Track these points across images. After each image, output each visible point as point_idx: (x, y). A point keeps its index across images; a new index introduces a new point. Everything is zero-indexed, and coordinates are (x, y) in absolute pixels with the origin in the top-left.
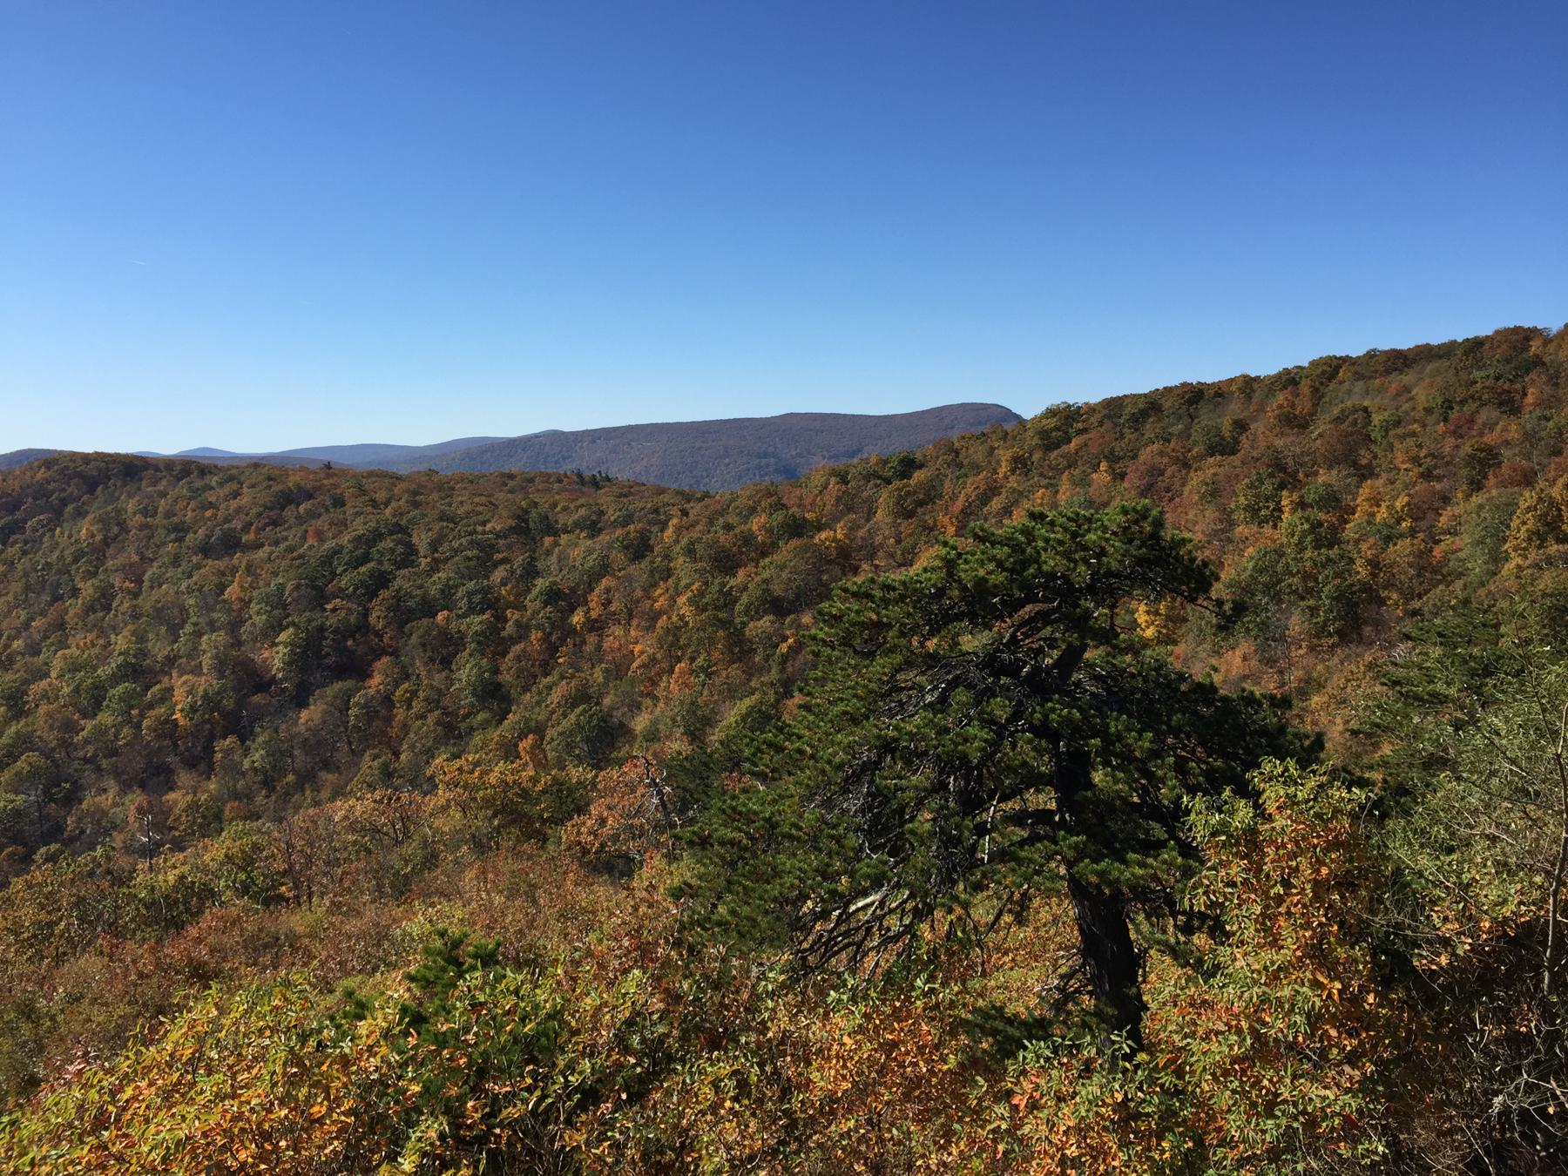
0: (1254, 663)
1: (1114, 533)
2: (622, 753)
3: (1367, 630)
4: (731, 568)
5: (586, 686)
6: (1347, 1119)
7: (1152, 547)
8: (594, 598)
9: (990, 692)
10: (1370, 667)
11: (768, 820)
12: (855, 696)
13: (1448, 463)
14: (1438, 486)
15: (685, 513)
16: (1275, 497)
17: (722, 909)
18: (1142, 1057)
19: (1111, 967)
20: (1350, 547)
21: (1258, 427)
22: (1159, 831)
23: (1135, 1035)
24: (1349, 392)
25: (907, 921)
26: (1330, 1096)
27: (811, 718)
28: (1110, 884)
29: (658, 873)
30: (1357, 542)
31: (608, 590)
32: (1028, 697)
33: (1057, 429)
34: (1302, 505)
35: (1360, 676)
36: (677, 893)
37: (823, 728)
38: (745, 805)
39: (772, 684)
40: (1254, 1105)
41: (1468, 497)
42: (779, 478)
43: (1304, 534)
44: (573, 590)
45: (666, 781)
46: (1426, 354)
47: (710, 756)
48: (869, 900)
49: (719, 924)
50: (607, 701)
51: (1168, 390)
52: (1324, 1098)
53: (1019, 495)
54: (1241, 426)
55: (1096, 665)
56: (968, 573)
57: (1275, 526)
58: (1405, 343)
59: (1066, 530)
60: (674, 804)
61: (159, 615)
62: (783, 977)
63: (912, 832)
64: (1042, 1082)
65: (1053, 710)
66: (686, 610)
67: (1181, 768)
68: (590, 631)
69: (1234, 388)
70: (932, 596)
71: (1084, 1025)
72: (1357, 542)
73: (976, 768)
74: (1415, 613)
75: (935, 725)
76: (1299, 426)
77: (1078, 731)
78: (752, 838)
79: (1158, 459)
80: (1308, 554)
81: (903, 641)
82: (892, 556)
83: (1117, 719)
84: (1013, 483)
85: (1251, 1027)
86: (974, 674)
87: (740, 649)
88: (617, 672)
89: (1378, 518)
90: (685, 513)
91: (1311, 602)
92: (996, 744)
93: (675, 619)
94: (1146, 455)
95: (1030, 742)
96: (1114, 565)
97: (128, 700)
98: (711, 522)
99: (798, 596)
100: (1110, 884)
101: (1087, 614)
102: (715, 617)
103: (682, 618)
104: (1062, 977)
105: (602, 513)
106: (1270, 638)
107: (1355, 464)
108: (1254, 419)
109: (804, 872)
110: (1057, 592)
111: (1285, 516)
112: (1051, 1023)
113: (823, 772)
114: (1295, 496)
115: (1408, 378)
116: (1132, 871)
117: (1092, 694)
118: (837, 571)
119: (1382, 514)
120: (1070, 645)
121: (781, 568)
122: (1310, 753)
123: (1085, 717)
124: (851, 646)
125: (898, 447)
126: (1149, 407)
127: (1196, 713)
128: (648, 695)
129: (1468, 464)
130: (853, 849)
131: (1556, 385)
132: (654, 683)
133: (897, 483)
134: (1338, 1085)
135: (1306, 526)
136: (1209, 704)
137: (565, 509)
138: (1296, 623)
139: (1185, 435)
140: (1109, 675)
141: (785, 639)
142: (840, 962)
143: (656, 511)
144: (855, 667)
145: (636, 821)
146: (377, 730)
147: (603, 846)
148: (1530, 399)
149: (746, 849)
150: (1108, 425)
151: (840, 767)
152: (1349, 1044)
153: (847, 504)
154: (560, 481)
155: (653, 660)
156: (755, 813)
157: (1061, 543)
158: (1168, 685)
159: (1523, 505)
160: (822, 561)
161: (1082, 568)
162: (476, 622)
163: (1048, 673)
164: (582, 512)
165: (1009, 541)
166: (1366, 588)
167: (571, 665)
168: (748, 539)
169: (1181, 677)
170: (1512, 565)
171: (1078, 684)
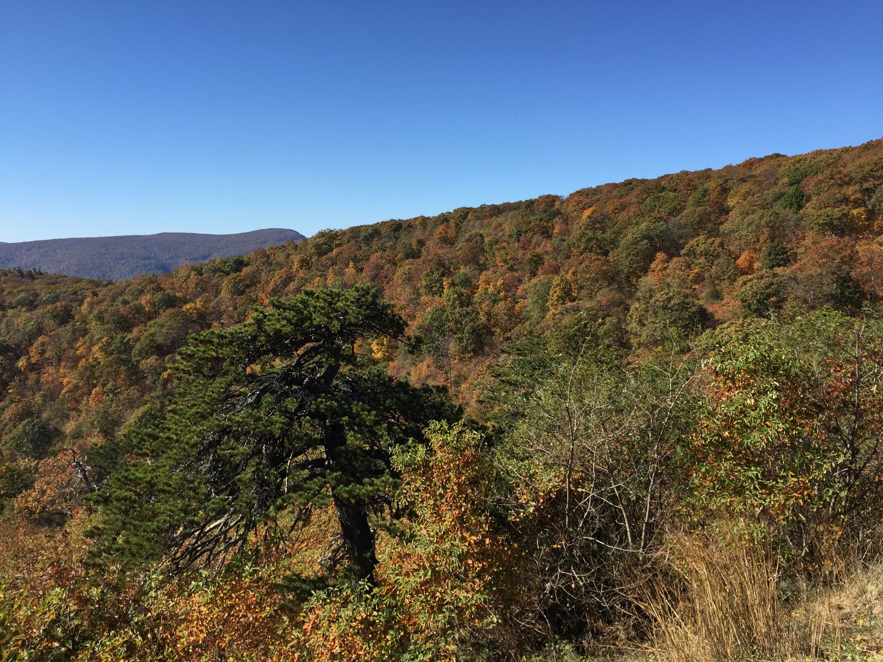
0: (433, 368)
1: (352, 302)
2: (57, 448)
3: (487, 349)
4: (129, 327)
5: (29, 406)
6: (478, 607)
7: (372, 310)
8: (33, 350)
9: (286, 394)
10: (488, 367)
11: (149, 482)
12: (204, 402)
14: (516, 274)
15: (95, 294)
16: (440, 281)
17: (120, 540)
18: (376, 590)
19: (358, 542)
21: (430, 243)
22: (382, 464)
23: (371, 580)
24: (473, 226)
25: (241, 532)
26: (468, 596)
27: (177, 417)
29: (79, 523)
30: (480, 303)
31: (43, 344)
32: (307, 396)
33: (324, 244)
38: (133, 474)
39: (158, 397)
40: (432, 607)
41: (530, 279)
42: (156, 272)
44: (18, 345)
45: (88, 463)
47: (117, 445)
48: (217, 523)
49: (117, 550)
50: (45, 415)
51: (384, 223)
52: (466, 598)
53: (306, 281)
54: (421, 243)
55: (345, 375)
57: (440, 296)
58: (498, 202)
59: (325, 301)
60: (93, 477)
62: (161, 577)
63: (239, 480)
64: (321, 613)
66: (99, 355)
68: (31, 371)
70: (249, 341)
71: (346, 576)
72: (480, 303)
73: (279, 438)
74: (508, 339)
75: (253, 416)
76: (450, 243)
77: (336, 413)
78: (138, 494)
79: (380, 261)
80: (457, 310)
81: (233, 368)
82: (232, 317)
83: (357, 405)
84: (301, 274)
85: (431, 566)
86: (276, 385)
87: (136, 377)
88: (52, 396)
90: (95, 294)
91: (459, 335)
92: (290, 424)
93: (91, 360)
94: (373, 258)
95: (308, 421)
96: (353, 320)
98: (114, 299)
99: (173, 343)
100: (354, 497)
101: (339, 348)
102: (119, 358)
103: (96, 359)
105: (37, 295)
106: (440, 354)
108: (428, 239)
109: (173, 512)
110: (323, 336)
111: (445, 291)
112: (327, 579)
113: (184, 449)
114: (450, 280)
115: (500, 219)
116: (365, 489)
117: (344, 391)
118: (198, 327)
119: (491, 289)
120: (330, 365)
121: (161, 327)
122: (453, 416)
123: (340, 405)
124: (201, 372)
125: (233, 254)
126: (374, 233)
127: (398, 399)
128: (73, 409)
129: (529, 263)
130: (204, 494)
131: (567, 224)
132: (78, 401)
133: (233, 275)
135: (456, 296)
136: (406, 393)
137: (9, 293)
138: (453, 346)
139: (393, 248)
140: (353, 381)
141: (165, 369)
142: (199, 562)
143: (75, 293)
144: (203, 385)
145: (67, 490)
147: (44, 508)
148: (556, 231)
149: (135, 501)
150: (353, 242)
151: (195, 445)
153: (203, 287)
154: (6, 275)
155: (77, 387)
156: (140, 479)
157: (323, 308)
158: (384, 384)
159: (555, 283)
160: (188, 322)
161: (335, 322)
163: (318, 382)
164: (22, 295)
165: (292, 308)
166: (485, 327)
167: (18, 394)
168: (139, 309)
169: (391, 379)
171: (337, 386)
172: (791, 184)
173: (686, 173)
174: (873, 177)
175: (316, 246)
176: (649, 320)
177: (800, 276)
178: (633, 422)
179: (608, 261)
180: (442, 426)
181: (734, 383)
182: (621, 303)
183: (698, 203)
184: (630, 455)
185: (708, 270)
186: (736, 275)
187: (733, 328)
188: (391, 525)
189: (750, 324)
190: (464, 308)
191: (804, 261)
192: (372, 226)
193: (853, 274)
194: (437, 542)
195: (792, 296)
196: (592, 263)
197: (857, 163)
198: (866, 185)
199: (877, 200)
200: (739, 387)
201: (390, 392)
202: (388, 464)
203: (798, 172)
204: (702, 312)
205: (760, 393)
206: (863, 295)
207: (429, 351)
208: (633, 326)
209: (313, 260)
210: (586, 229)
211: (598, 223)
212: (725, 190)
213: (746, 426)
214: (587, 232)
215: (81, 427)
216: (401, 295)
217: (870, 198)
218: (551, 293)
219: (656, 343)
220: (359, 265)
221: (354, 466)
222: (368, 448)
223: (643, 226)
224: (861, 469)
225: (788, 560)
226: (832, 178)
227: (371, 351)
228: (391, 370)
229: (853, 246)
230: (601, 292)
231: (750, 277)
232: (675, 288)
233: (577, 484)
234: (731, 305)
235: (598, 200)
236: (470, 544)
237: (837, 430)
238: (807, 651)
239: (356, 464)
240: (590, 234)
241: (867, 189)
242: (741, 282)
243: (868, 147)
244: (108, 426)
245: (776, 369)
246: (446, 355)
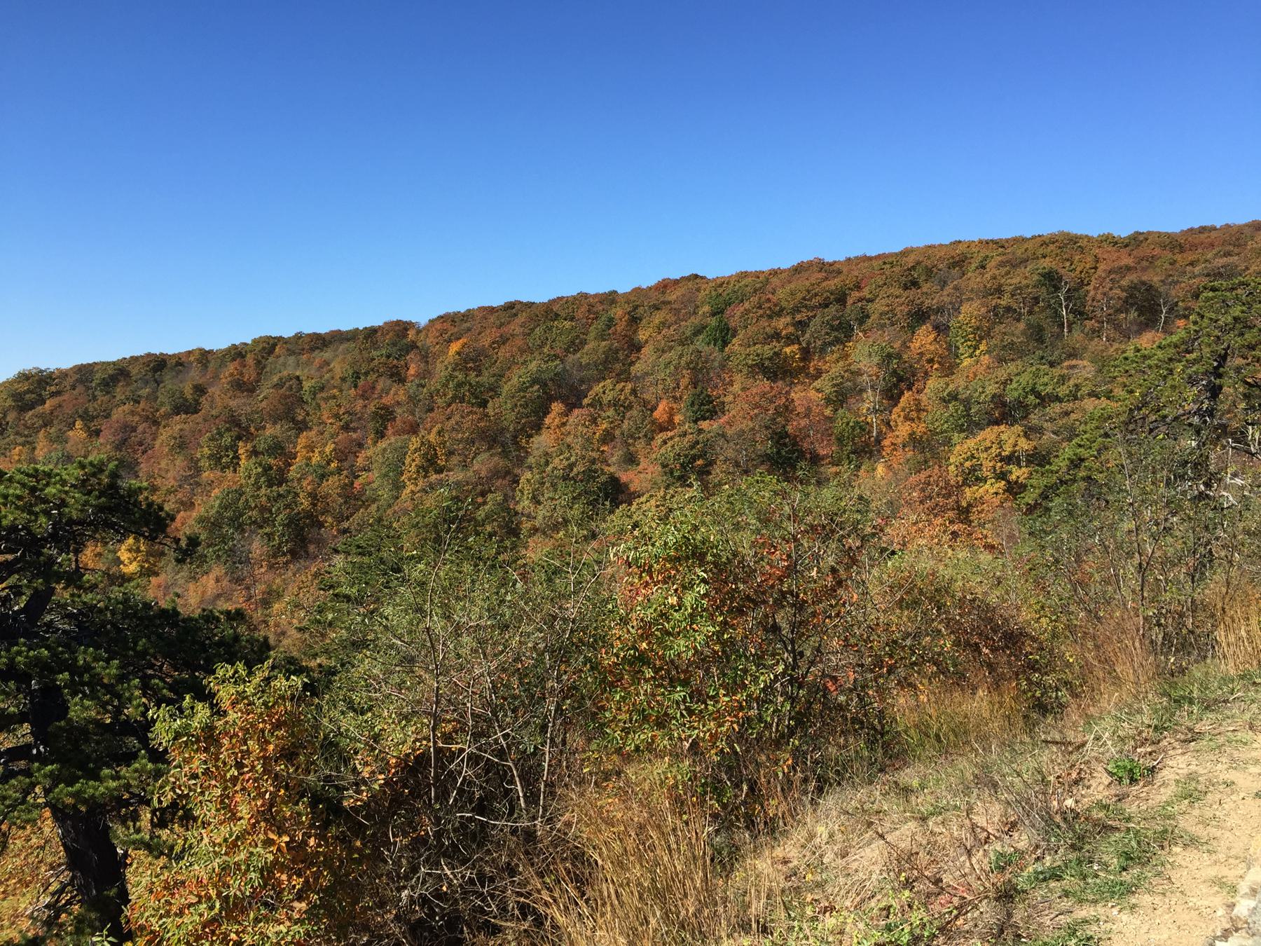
0: (225, 583)
1: (73, 486)
3: (312, 548)
10: (316, 575)
13: (360, 419)
14: (354, 436)
16: (234, 448)
20: (295, 484)
22: (133, 742)
24: (284, 365)
28: (85, 802)
33: (29, 391)
34: (255, 453)
35: (309, 584)
43: (258, 476)
51: (134, 359)
54: (200, 390)
55: (66, 604)
57: (235, 471)
58: (323, 329)
59: (24, 485)
65: (19, 653)
69: (192, 359)
72: (299, 480)
74: (345, 531)
79: (129, 418)
80: (263, 491)
83: (85, 652)
85: (219, 894)
89: (314, 461)
91: (268, 530)
94: (118, 414)
100: (85, 802)
101: (51, 561)
104: (53, 894)
106: (236, 560)
107: (293, 420)
108: (211, 385)
110: (20, 543)
114: (249, 446)
115: (327, 355)
117: (64, 631)
119: (316, 458)
122: (257, 653)
123: (54, 655)
126: (118, 373)
129: (373, 419)
131: (427, 362)
134: (290, 919)
135: (260, 470)
136: (174, 625)
138: (257, 547)
139: (153, 397)
148: (412, 371)
152: (298, 882)
157: (19, 498)
159: (412, 448)
163: (15, 619)
166: (309, 515)
170: (407, 491)
172: (714, 314)
173: (584, 296)
174: (806, 307)
175: (13, 396)
176: (546, 496)
177: (730, 432)
178: (528, 639)
179: (487, 415)
180: (236, 672)
181: (651, 577)
182: (508, 473)
183: (602, 337)
184: (522, 691)
185: (619, 426)
186: (653, 431)
187: (653, 502)
188: (151, 838)
189: (673, 496)
190: (275, 488)
191: (733, 412)
192: (114, 363)
193: (789, 428)
194: (226, 854)
195: (722, 458)
196: (465, 419)
197: (788, 288)
198: (798, 317)
199: (812, 335)
200: (659, 581)
201: (147, 627)
202: (145, 741)
203: (721, 299)
204: (614, 480)
205: (684, 587)
206: (802, 455)
207: (218, 557)
208: (525, 504)
209: (8, 419)
210: (454, 370)
211: (471, 361)
212: (634, 320)
213: (668, 634)
214: (456, 373)
216: (168, 471)
217: (804, 333)
218: (407, 462)
219: (556, 527)
220: (93, 425)
221: (83, 751)
222: (108, 721)
223: (533, 366)
224: (804, 676)
225: (724, 806)
226: (760, 307)
227: (118, 562)
228: (155, 592)
229: (788, 393)
230: (479, 458)
231: (670, 434)
232: (578, 450)
233: (448, 738)
234: (649, 471)
235: (469, 330)
236: (279, 849)
237: (776, 628)
238: (745, 927)
239: (87, 749)
240: (460, 376)
241: (800, 322)
242: (659, 441)
243: (799, 269)
245: (704, 555)
246: (248, 561)
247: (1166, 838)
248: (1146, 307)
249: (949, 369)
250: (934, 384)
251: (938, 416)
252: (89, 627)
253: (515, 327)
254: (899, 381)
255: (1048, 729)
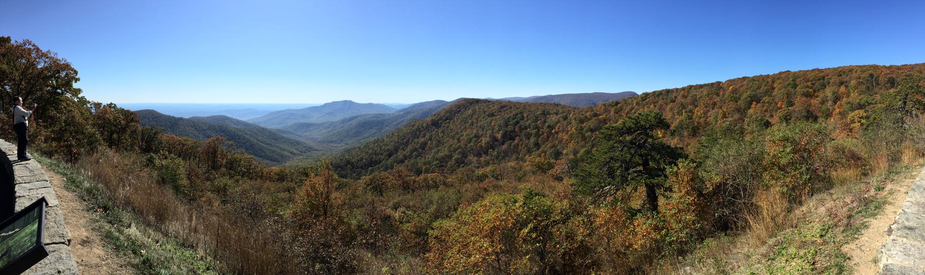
19: (652, 199)
26: (690, 217)
36: (572, 185)
37: (600, 153)
46: (705, 85)
53: (637, 110)
56: (627, 125)
61: (480, 127)
67: (664, 161)
77: (647, 155)
87: (584, 138)
88: (560, 142)
97: (475, 141)
106: (681, 136)
116: (655, 181)
121: (592, 123)
125: (615, 100)
138: (686, 133)
146: (516, 150)
153: (606, 111)
160: (600, 121)
162: (534, 131)
168: (586, 117)
196: (732, 105)
211: (735, 91)
215: (568, 152)
228: (664, 140)
243: (813, 70)
244: (575, 153)
247: (885, 203)
248: (892, 83)
249: (848, 96)
250: (844, 99)
251: (846, 107)
252: (653, 148)
253: (745, 83)
254: (837, 99)
255: (864, 179)
